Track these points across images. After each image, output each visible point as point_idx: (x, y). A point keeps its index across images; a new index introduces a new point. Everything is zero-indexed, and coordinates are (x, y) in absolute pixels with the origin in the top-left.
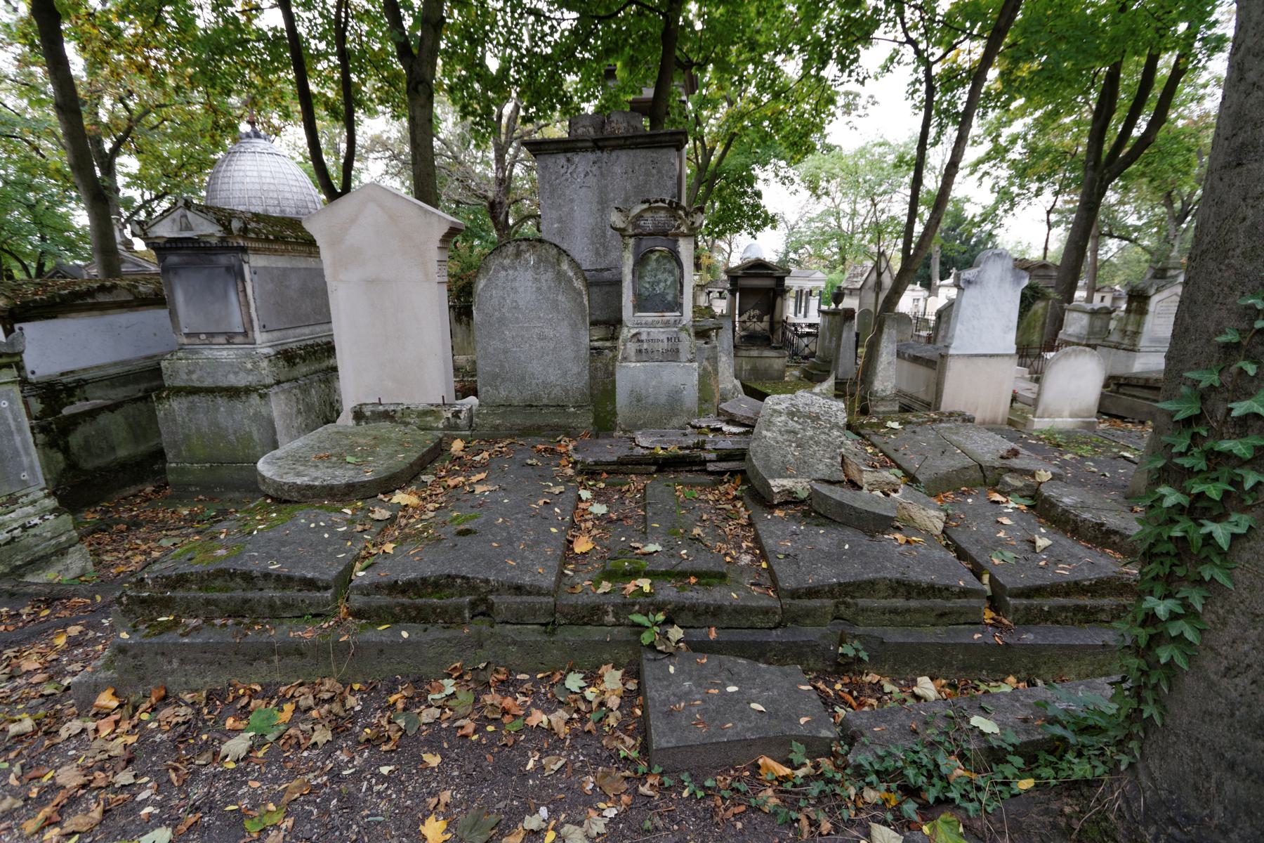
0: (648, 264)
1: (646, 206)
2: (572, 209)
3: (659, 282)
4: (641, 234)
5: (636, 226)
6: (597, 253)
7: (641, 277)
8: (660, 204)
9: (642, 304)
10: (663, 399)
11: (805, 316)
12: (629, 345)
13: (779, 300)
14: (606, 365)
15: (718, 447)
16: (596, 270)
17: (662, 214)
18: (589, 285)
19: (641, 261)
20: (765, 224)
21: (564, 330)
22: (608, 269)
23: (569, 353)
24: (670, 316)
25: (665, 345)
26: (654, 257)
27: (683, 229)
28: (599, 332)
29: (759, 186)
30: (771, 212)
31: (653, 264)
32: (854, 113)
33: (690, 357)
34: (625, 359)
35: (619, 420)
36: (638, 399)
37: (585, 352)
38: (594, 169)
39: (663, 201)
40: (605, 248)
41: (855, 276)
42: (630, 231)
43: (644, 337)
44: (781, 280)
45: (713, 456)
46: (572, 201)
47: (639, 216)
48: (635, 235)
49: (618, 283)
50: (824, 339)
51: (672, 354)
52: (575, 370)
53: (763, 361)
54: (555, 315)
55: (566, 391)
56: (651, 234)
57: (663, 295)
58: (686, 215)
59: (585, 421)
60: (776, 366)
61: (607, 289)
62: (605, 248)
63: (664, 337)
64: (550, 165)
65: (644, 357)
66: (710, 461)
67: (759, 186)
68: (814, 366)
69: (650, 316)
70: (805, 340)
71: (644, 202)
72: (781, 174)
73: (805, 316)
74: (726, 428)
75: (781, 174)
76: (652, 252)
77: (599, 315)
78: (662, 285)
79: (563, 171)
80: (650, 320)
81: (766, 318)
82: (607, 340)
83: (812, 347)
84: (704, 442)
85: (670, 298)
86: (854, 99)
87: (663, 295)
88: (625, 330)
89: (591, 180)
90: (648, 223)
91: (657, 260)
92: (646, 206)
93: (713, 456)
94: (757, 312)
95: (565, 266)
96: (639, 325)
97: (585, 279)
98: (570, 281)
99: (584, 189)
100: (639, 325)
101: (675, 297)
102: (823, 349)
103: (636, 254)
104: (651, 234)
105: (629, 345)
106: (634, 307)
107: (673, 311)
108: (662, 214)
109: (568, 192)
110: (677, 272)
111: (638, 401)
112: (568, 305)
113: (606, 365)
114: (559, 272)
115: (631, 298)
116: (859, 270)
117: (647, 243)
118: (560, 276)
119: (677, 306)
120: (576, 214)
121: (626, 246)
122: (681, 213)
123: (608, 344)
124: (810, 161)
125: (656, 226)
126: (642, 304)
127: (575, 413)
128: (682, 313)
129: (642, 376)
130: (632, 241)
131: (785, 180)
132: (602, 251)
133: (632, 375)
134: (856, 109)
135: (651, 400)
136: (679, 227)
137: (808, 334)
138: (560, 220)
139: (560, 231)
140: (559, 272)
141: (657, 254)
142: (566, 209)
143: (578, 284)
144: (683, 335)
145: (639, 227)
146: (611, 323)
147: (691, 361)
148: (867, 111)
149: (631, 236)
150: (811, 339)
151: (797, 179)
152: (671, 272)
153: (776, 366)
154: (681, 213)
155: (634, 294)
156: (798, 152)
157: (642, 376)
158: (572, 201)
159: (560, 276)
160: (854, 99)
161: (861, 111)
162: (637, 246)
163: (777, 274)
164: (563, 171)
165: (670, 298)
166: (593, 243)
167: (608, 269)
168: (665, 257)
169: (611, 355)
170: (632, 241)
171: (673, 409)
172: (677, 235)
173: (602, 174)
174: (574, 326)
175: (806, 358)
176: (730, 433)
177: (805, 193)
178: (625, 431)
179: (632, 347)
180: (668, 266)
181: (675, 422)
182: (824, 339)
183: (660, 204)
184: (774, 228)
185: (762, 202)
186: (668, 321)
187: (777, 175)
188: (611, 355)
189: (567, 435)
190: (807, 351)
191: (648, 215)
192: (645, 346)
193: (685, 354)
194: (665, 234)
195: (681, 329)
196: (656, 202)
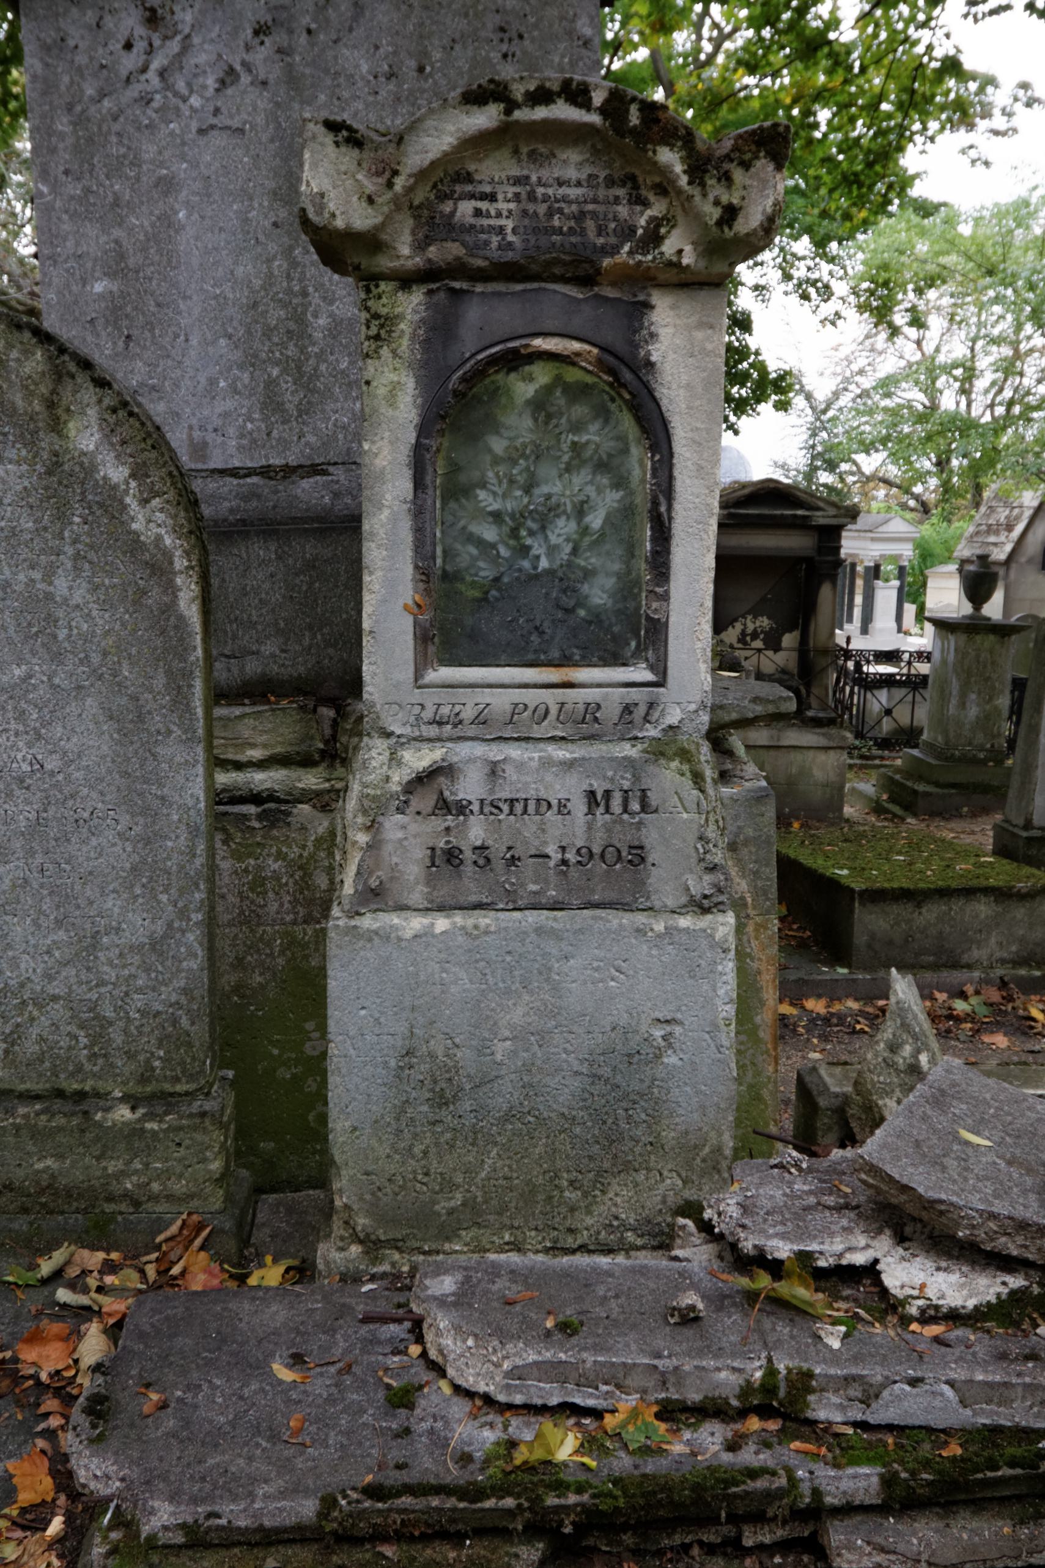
0: (493, 425)
1: (486, 118)
2: (167, 220)
3: (546, 516)
4: (458, 270)
5: (433, 226)
6: (271, 403)
7: (457, 491)
8: (563, 111)
9: (454, 627)
10: (563, 1092)
11: (865, 630)
12: (394, 826)
13: (825, 591)
14: (304, 869)
15: (882, 1413)
16: (266, 472)
17: (571, 166)
18: (208, 535)
19: (456, 409)
20: (759, 396)
21: (86, 737)
22: (315, 470)
23: (107, 849)
24: (601, 682)
25: (576, 828)
26: (524, 387)
27: (679, 245)
28: (262, 732)
29: (744, 300)
30: (774, 366)
31: (518, 426)
32: (982, 124)
33: (700, 884)
34: (374, 896)
35: (345, 1189)
36: (436, 1089)
37: (182, 839)
38: (261, 55)
39: (578, 95)
40: (305, 381)
41: (990, 530)
42: (404, 252)
43: (470, 787)
44: (831, 535)
45: (861, 1481)
46: (167, 185)
47: (451, 175)
48: (427, 276)
49: (345, 527)
50: (943, 696)
51: (612, 874)
52: (139, 926)
53: (797, 757)
54: (39, 668)
55: (97, 1028)
56: (509, 272)
57: (566, 581)
58: (700, 167)
59: (192, 1167)
60: (818, 774)
61: (310, 549)
62: (305, 381)
63: (571, 789)
64: (76, 36)
65: (471, 887)
66: (848, 1509)
67: (744, 300)
68: (917, 770)
69: (499, 685)
70: (883, 695)
71: (475, 98)
72: (800, 272)
73: (865, 630)
74: (906, 1274)
75: (800, 272)
76: (515, 360)
77: (269, 656)
78: (563, 529)
79: (129, 62)
80: (501, 701)
81: (789, 640)
82: (306, 762)
83: (902, 715)
84: (802, 1382)
85: (599, 594)
86: (981, 90)
87: (566, 581)
88: (374, 754)
89: (249, 104)
90: (497, 213)
91: (539, 405)
92: (486, 118)
93: (861, 1481)
94: (764, 622)
95: (86, 435)
96: (447, 726)
97: (189, 502)
98: (111, 504)
99: (218, 140)
100: (447, 726)
101: (628, 588)
102: (940, 720)
103: (431, 369)
104: (509, 272)
105: (394, 826)
106: (423, 637)
107: (615, 659)
108: (571, 166)
109: (149, 151)
110: (639, 464)
111: (441, 1101)
112: (102, 620)
113: (304, 869)
114: (55, 466)
115: (407, 591)
116: (1002, 515)
117: (486, 319)
118: (63, 481)
119: (637, 634)
120: (184, 241)
121: (381, 329)
122: (669, 157)
123: (311, 780)
124: (891, 231)
125: (534, 227)
126: (454, 627)
127: (135, 1132)
128: (661, 669)
129: (461, 983)
130: (410, 306)
131: (809, 290)
132: (291, 398)
133: (406, 979)
134: (986, 115)
135: (504, 1095)
136: (653, 238)
137: (888, 681)
138: (117, 264)
139: (115, 312)
140: (55, 466)
141: (542, 375)
142: (140, 221)
143: (153, 522)
144: (668, 779)
145: (450, 229)
146: (327, 700)
147: (702, 906)
148: (1015, 122)
149: (406, 281)
150: (899, 693)
151: (841, 288)
152: (607, 466)
153: (818, 774)
154: (669, 157)
155: (424, 573)
156: (860, 202)
157: (461, 983)
158: (167, 185)
159: (63, 481)
160: (981, 90)
161: (999, 122)
162: (439, 331)
163: (821, 519)
164: (129, 62)
165: (599, 594)
166: (252, 361)
167: (315, 470)
168: (578, 392)
169: (321, 825)
170: (410, 306)
171: (612, 1140)
172: (643, 280)
173: (292, 79)
174: (130, 723)
175: (885, 744)
176: (931, 1315)
177: (856, 324)
178: (373, 1246)
179: (408, 838)
180: (593, 435)
181: (622, 1201)
182: (943, 696)
183: (563, 111)
184: (783, 406)
185: (751, 342)
186: (592, 711)
187: (787, 277)
188: (321, 825)
189: (96, 1235)
190: (887, 725)
191: (495, 169)
192: (476, 831)
193: (672, 874)
194: (583, 272)
195: (659, 751)
196: (541, 96)
